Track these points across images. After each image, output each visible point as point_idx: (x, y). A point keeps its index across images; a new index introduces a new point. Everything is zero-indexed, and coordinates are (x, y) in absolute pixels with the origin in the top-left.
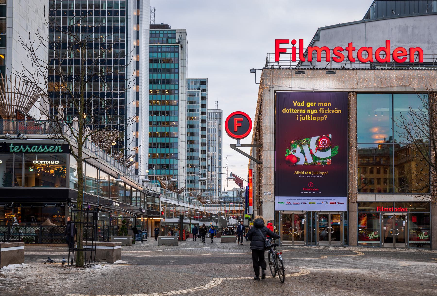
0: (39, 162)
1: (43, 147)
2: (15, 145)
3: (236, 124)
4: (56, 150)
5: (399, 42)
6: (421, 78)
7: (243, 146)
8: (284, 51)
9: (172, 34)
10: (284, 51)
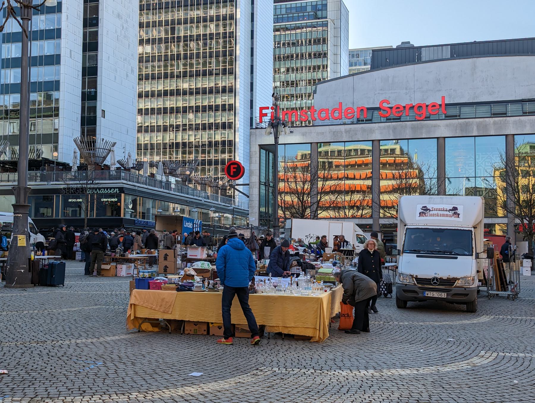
0: (105, 200)
1: (107, 190)
2: (90, 188)
3: (232, 170)
4: (115, 191)
5: (381, 90)
6: (364, 130)
7: (238, 185)
8: (266, 115)
9: (322, 4)
10: (266, 115)
